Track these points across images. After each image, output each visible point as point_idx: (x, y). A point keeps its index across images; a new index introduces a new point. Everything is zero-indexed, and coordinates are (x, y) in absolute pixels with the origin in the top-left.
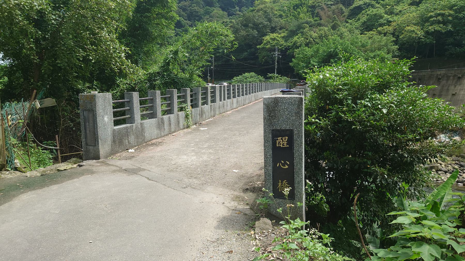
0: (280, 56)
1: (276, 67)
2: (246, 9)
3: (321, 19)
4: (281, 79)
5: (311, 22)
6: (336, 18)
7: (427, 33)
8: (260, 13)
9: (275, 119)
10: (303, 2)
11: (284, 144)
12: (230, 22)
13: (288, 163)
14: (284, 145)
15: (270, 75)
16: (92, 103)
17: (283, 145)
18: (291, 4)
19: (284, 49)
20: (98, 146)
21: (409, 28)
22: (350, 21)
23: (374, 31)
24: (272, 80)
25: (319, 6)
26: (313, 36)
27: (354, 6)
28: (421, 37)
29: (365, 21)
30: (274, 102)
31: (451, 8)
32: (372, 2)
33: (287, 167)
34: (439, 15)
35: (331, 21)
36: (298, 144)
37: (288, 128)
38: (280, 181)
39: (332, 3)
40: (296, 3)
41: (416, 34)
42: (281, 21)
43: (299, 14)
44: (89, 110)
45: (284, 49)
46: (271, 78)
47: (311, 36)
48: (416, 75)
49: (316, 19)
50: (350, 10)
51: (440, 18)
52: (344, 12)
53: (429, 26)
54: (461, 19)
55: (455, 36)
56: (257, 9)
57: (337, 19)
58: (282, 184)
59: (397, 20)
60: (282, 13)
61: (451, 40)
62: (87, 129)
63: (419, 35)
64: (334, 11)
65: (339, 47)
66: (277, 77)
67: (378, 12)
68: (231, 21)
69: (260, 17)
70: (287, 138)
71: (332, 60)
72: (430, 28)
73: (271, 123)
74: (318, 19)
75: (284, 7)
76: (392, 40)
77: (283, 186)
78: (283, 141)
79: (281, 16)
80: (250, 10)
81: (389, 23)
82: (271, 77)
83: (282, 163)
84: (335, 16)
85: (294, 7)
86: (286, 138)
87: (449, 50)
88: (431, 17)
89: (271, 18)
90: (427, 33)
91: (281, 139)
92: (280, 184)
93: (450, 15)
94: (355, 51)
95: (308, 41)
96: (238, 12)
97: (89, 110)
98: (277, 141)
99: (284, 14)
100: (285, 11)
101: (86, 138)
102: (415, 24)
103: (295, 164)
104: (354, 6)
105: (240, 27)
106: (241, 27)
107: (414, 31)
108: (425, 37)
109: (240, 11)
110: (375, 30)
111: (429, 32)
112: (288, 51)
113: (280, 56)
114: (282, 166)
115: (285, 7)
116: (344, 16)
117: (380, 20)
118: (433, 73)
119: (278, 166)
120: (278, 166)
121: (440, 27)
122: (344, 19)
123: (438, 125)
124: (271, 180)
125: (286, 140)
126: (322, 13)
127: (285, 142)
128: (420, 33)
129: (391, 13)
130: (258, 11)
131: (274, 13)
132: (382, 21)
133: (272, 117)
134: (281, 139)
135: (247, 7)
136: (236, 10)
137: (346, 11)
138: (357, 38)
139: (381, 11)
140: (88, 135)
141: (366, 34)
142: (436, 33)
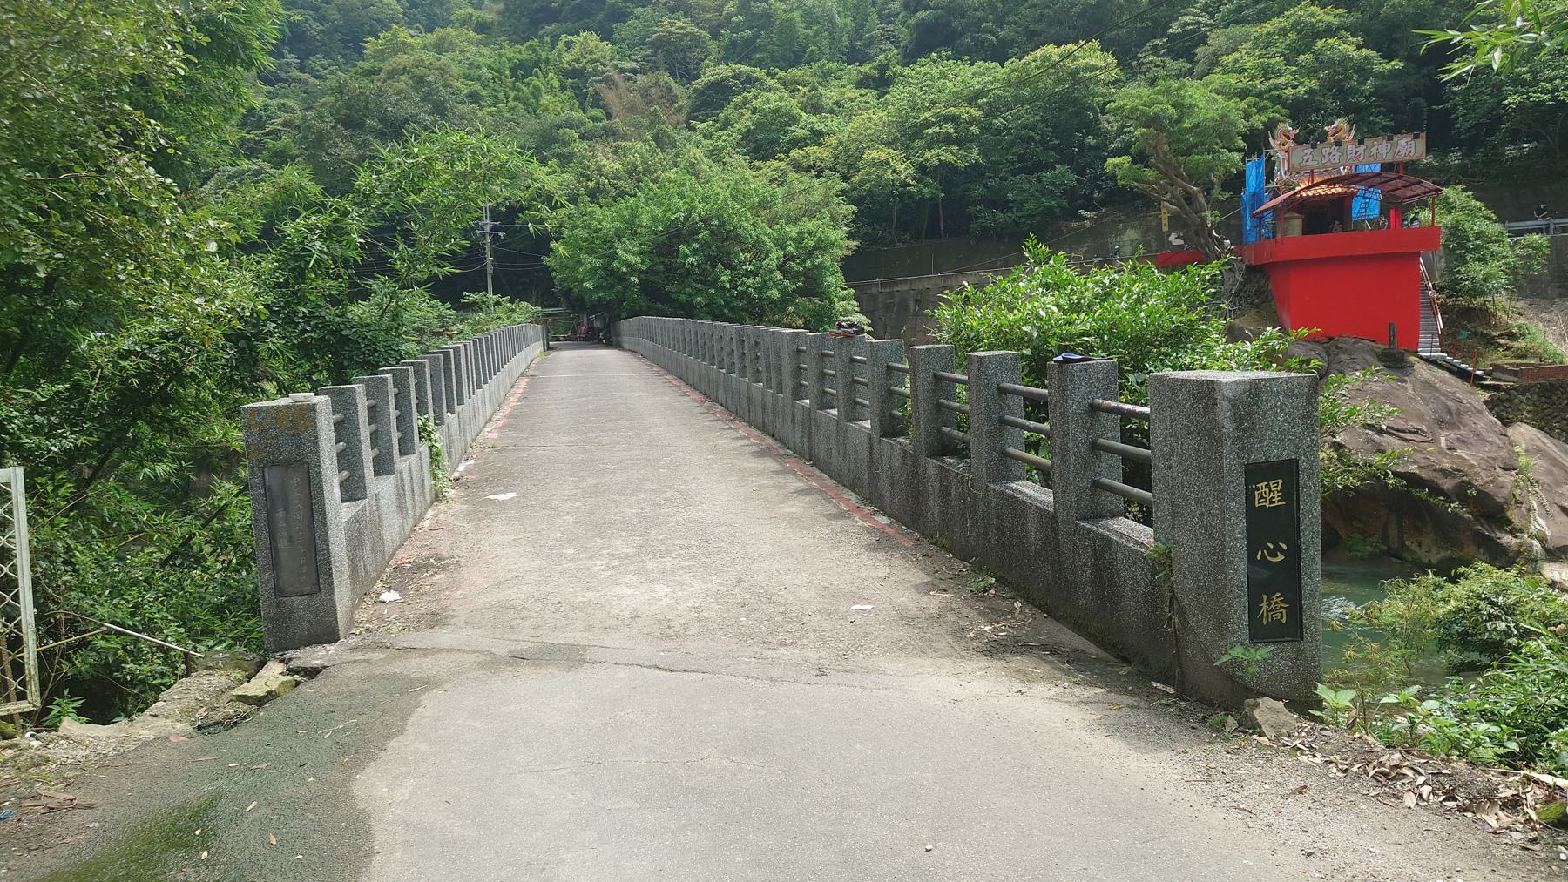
0: (500, 234)
1: (490, 270)
2: (324, 62)
3: (609, 116)
4: (513, 311)
5: (582, 123)
6: (659, 116)
7: (922, 169)
8: (403, 83)
9: (1251, 436)
10: (543, 57)
12: (279, 109)
13: (1285, 547)
15: (473, 297)
16: (299, 435)
17: (1271, 502)
18: (504, 59)
19: (503, 209)
20: (332, 592)
21: (874, 154)
22: (701, 126)
23: (780, 160)
24: (482, 315)
25: (596, 73)
26: (607, 170)
28: (908, 180)
29: (749, 130)
30: (1251, 393)
31: (972, 100)
32: (754, 72)
33: (1281, 557)
34: (946, 119)
35: (646, 122)
36: (1310, 496)
37: (1285, 457)
38: (1265, 597)
39: (636, 65)
40: (518, 56)
41: (894, 171)
42: (480, 114)
43: (536, 94)
44: (287, 464)
45: (503, 209)
46: (473, 307)
47: (600, 169)
49: (594, 112)
50: (696, 90)
51: (949, 128)
52: (676, 96)
53: (924, 149)
54: (999, 132)
55: (990, 177)
56: (386, 66)
57: (663, 118)
59: (840, 129)
60: (477, 87)
61: (978, 190)
63: (903, 176)
64: (646, 91)
65: (700, 206)
66: (497, 303)
67: (782, 104)
68: (283, 105)
69: (405, 98)
71: (684, 248)
72: (928, 155)
73: (1244, 448)
74: (599, 114)
75: (479, 67)
76: (838, 187)
78: (1270, 491)
79: (474, 98)
80: (361, 71)
81: (817, 137)
82: (474, 303)
84: (658, 108)
85: (513, 70)
87: (977, 218)
88: (927, 124)
89: (445, 101)
90: (922, 169)
91: (1267, 486)
92: (1264, 605)
93: (973, 121)
94: (747, 220)
95: (591, 184)
96: (296, 73)
97: (287, 464)
98: (1256, 493)
99: (484, 93)
100: (486, 83)
102: (888, 144)
103: (1303, 547)
105: (332, 127)
106: (334, 127)
108: (919, 181)
109: (302, 70)
110: (782, 156)
111: (926, 167)
112: (520, 215)
113: (500, 234)
114: (1269, 558)
115: (484, 69)
116: (680, 110)
117: (792, 128)
119: (1259, 557)
120: (1259, 557)
121: (951, 152)
122: (682, 117)
124: (1246, 599)
125: (1279, 489)
126: (610, 97)
127: (1277, 494)
128: (905, 170)
129: (815, 108)
130: (393, 74)
131: (451, 87)
132: (798, 131)
133: (1245, 430)
134: (1267, 486)
135: (327, 56)
136: (288, 64)
137: (684, 95)
138: (746, 181)
139: (792, 103)
140: (284, 556)
141: (759, 168)
142: (945, 172)
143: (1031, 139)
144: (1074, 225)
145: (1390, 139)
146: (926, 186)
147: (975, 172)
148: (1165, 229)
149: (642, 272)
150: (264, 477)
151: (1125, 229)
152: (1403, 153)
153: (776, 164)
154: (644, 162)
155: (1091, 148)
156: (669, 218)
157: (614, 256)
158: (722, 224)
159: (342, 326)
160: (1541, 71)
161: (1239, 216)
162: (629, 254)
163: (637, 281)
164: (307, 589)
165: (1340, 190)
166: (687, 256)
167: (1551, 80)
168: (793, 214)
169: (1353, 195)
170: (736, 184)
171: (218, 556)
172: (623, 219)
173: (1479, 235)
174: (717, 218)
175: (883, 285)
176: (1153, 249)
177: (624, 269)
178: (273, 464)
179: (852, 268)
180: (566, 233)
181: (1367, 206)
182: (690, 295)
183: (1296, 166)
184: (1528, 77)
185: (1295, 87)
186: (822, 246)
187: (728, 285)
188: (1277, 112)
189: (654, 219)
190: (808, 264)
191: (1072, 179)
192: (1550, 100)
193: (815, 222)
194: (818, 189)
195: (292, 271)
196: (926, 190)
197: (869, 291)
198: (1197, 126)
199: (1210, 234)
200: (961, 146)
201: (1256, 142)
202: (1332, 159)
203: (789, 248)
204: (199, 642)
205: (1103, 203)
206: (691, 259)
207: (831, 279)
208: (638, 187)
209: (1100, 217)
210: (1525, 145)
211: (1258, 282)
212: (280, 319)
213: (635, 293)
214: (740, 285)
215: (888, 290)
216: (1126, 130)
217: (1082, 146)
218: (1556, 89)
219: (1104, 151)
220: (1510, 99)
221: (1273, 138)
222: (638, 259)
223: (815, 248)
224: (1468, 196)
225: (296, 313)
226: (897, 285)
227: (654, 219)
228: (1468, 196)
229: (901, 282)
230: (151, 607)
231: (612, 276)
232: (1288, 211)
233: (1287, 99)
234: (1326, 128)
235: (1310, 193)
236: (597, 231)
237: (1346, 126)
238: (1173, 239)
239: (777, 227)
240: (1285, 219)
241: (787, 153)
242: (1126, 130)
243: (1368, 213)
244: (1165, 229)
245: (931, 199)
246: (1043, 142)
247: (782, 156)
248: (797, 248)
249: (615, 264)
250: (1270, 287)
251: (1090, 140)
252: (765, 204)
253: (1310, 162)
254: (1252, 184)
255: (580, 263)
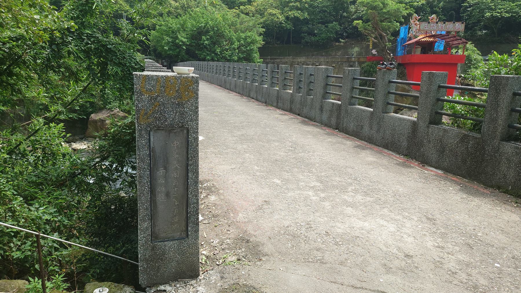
7: (287, 18)
16: (183, 105)
20: (197, 238)
23: (236, 9)
28: (282, 22)
41: (278, 18)
44: (170, 130)
48: (279, 61)
54: (315, 7)
61: (305, 28)
62: (158, 189)
63: (281, 20)
65: (210, 22)
71: (203, 37)
72: (290, 13)
90: (287, 18)
101: (153, 217)
102: (276, 8)
107: (275, 14)
111: (289, 17)
118: (294, 60)
121: (298, 13)
128: (282, 18)
140: (161, 207)
143: (325, 11)
144: (337, 44)
145: (454, 23)
146: (288, 25)
147: (306, 22)
148: (371, 48)
149: (187, 45)
150: (150, 139)
151: (355, 47)
152: (457, 28)
153: (235, 10)
154: (188, 4)
155: (344, 17)
156: (198, 26)
157: (177, 38)
158: (218, 30)
159: (107, 43)
160: (497, 6)
161: (396, 46)
162: (182, 38)
163: (185, 48)
164: (177, 235)
165: (432, 39)
166: (205, 41)
167: (500, 9)
168: (243, 29)
169: (436, 42)
170: (224, 15)
171: (33, 153)
172: (180, 24)
173: (475, 59)
174: (217, 27)
175: (271, 59)
176: (363, 55)
177: (181, 43)
178: (158, 128)
179: (262, 51)
180: (158, 27)
181: (440, 46)
182: (205, 55)
183: (422, 29)
184: (493, 7)
185: (418, 2)
186: (253, 42)
187: (219, 53)
188: (411, 10)
189: (193, 25)
190: (248, 48)
191: (338, 28)
192: (500, 16)
193: (251, 33)
194: (250, 21)
195: (81, 11)
196: (288, 26)
197: (266, 61)
198: (388, 11)
199: (387, 51)
200: (302, 11)
201: (407, 19)
202: (434, 28)
203: (242, 42)
204: (31, 205)
205: (347, 37)
206: (206, 42)
207: (256, 55)
208: (185, 13)
209: (346, 42)
210: (484, 31)
211: (402, 69)
212: (74, 36)
213: (183, 53)
214: (223, 54)
215: (272, 61)
216: (358, 12)
217: (341, 16)
218: (502, 12)
219: (349, 19)
220: (487, 14)
221: (411, 19)
222: (186, 40)
223: (251, 43)
224: (473, 46)
225: (83, 34)
226: (276, 59)
227: (193, 25)
228: (473, 46)
229: (277, 58)
230: (5, 187)
231: (175, 45)
232: (416, 45)
233: (415, 6)
234: (429, 17)
235: (422, 40)
236: (170, 28)
237: (435, 17)
238: (374, 52)
239: (237, 33)
240: (416, 48)
241: (239, 7)
242: (358, 12)
243: (439, 48)
244: (371, 48)
245: (290, 29)
246: (330, 13)
247: (237, 8)
248: (244, 42)
249: (177, 41)
250: (406, 71)
251: (345, 14)
252: (233, 24)
253: (426, 29)
254: (402, 35)
255: (163, 39)
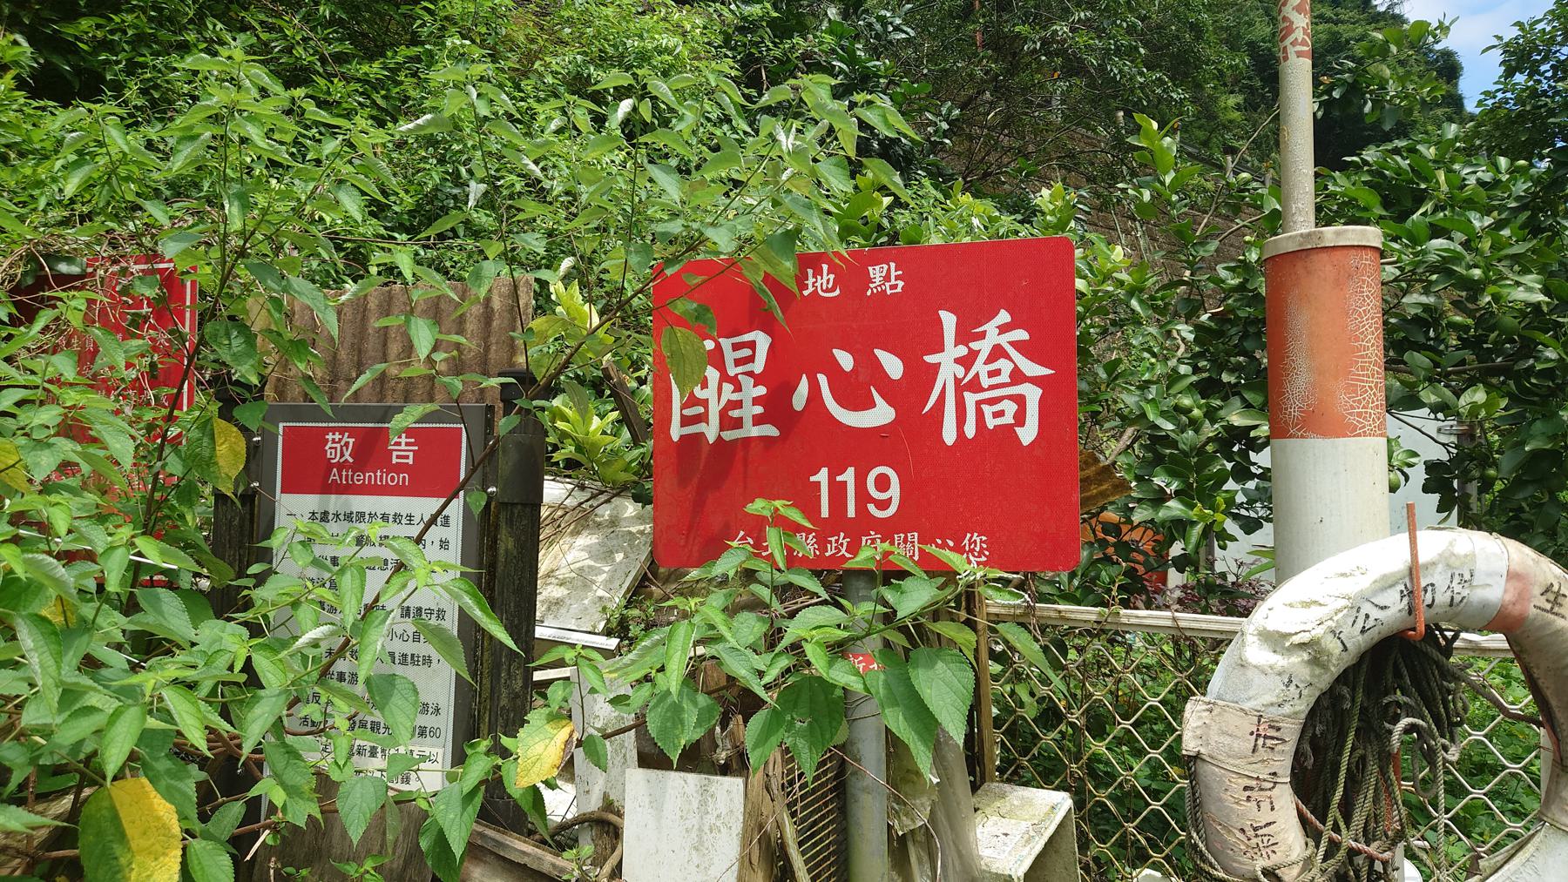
11: (738, 404)
14: (738, 423)
27: (704, 456)
38: (949, 320)
58: (967, 361)
70: (762, 341)
77: (975, 386)
83: (834, 370)
86: (752, 345)
104: (704, 456)
123: (1189, 769)
125: (758, 366)
